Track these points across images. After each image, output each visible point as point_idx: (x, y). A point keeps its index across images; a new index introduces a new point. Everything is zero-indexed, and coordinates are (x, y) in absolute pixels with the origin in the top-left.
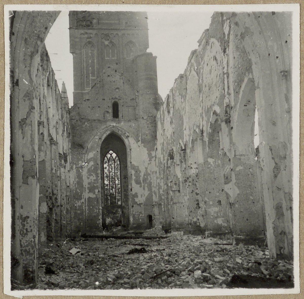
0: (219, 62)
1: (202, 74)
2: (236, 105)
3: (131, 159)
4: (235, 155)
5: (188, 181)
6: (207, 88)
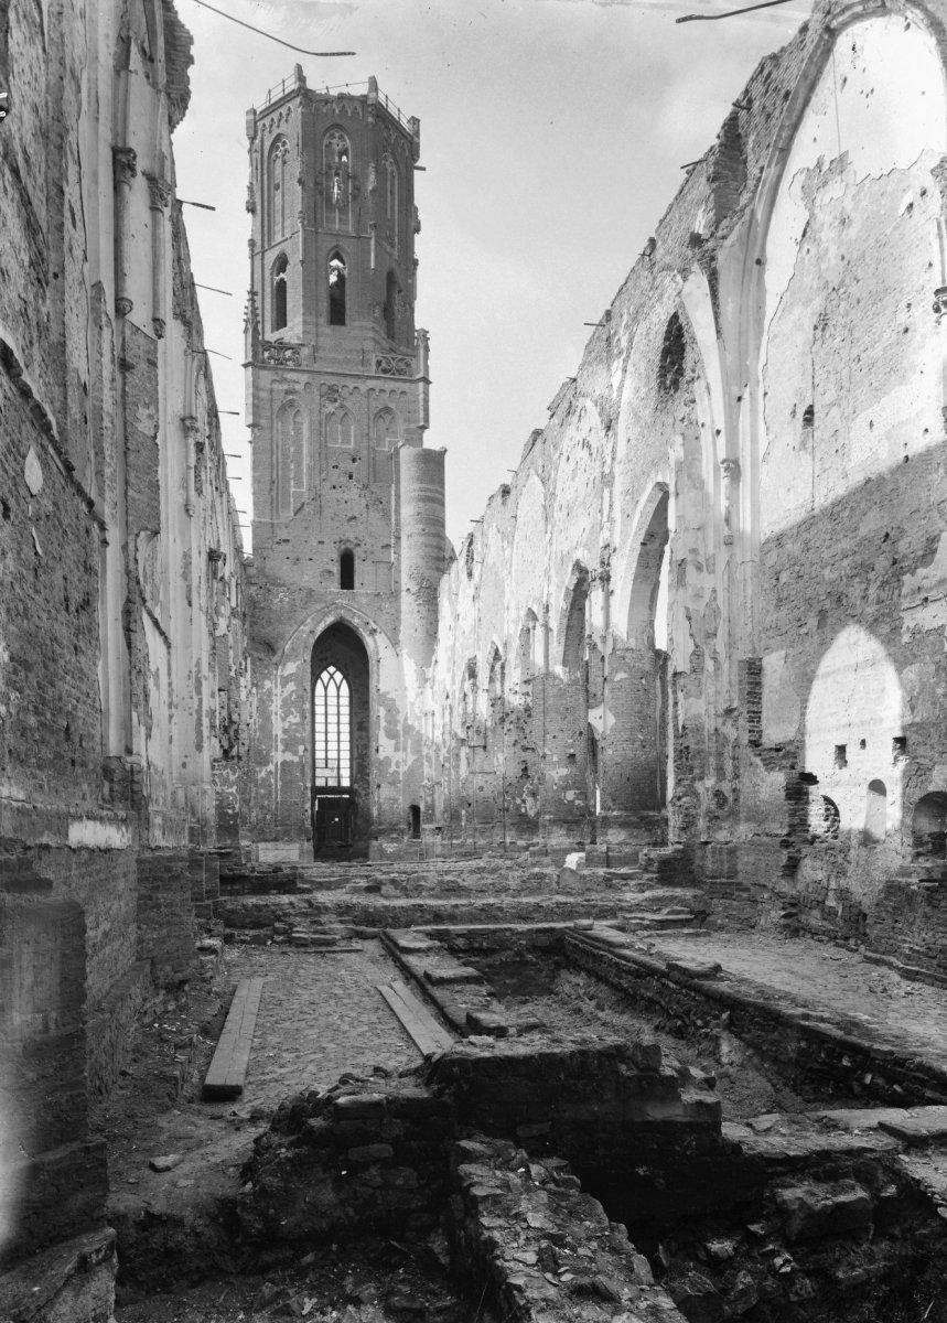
0: (594, 451)
1: (555, 481)
2: (624, 542)
3: (378, 682)
4: (614, 649)
5: (508, 720)
6: (565, 512)
